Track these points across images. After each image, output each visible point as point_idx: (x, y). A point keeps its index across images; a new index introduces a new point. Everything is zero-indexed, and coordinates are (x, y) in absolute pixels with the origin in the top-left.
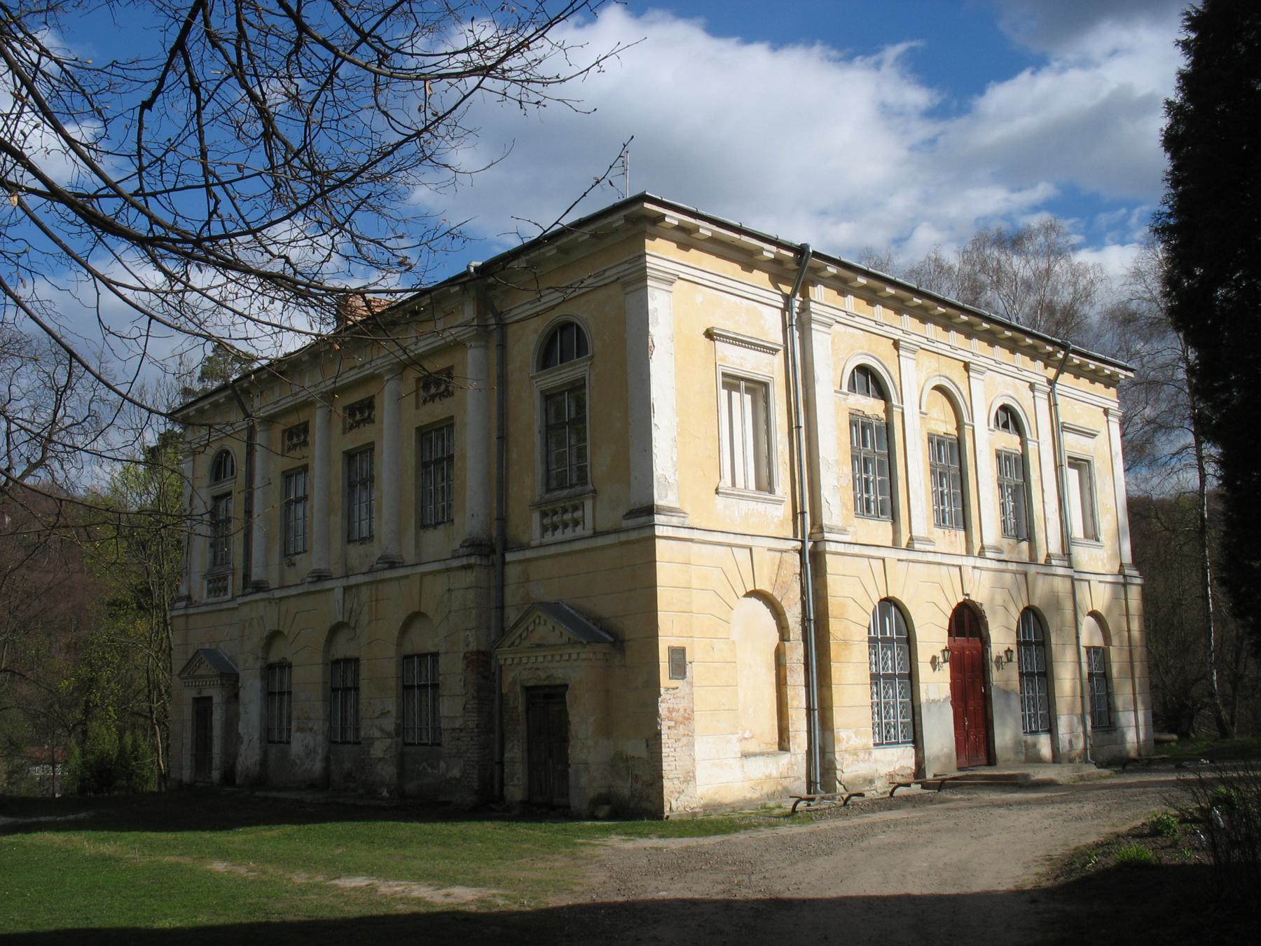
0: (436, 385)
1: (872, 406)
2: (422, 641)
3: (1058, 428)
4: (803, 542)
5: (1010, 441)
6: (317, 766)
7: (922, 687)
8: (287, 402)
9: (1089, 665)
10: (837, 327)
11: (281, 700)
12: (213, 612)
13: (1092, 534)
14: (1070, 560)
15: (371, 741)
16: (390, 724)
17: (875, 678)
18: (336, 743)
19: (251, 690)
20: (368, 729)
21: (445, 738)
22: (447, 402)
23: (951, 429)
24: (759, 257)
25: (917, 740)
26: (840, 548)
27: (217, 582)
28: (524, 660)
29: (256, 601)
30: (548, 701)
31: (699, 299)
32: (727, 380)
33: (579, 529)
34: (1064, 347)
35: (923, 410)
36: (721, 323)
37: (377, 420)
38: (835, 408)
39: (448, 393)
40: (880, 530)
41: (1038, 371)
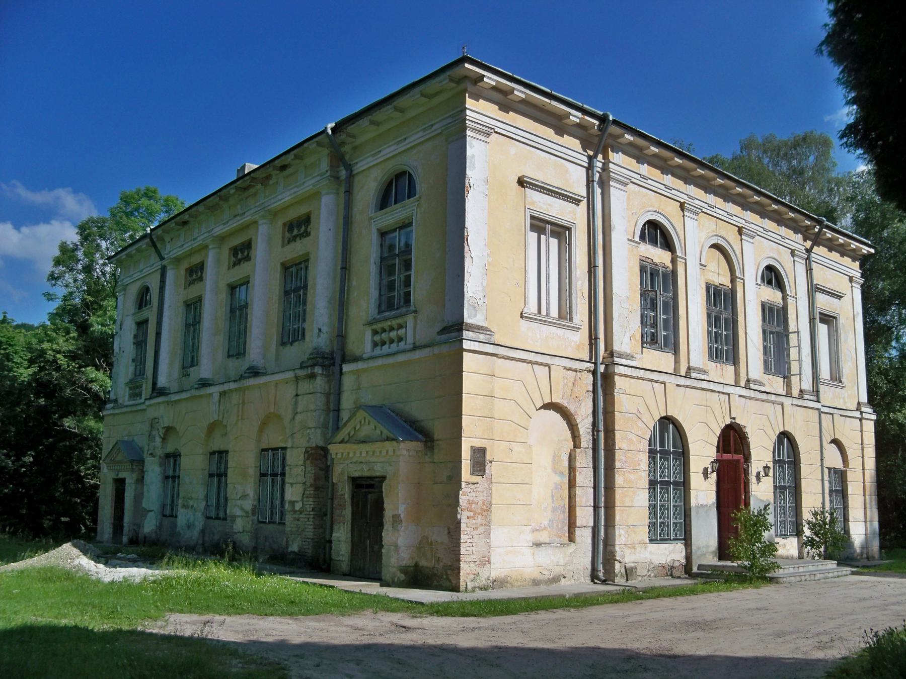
0: (299, 228)
1: (660, 256)
2: (274, 439)
3: (814, 289)
4: (595, 364)
5: (773, 296)
6: (195, 534)
7: (693, 494)
8: (187, 248)
9: (830, 483)
10: (631, 186)
11: (174, 481)
12: (132, 412)
13: (836, 378)
14: (818, 396)
15: (234, 518)
16: (248, 505)
17: (652, 483)
18: (211, 518)
19: (154, 471)
20: (234, 509)
21: (289, 518)
22: (305, 241)
23: (726, 280)
24: (566, 121)
25: (687, 540)
26: (628, 371)
27: (135, 388)
28: (351, 455)
29: (159, 403)
30: (368, 492)
31: (513, 151)
32: (535, 222)
33: (402, 344)
34: (819, 222)
35: (703, 263)
36: (531, 173)
37: (253, 258)
38: (627, 257)
39: (307, 234)
40: (662, 360)
41: (797, 240)
